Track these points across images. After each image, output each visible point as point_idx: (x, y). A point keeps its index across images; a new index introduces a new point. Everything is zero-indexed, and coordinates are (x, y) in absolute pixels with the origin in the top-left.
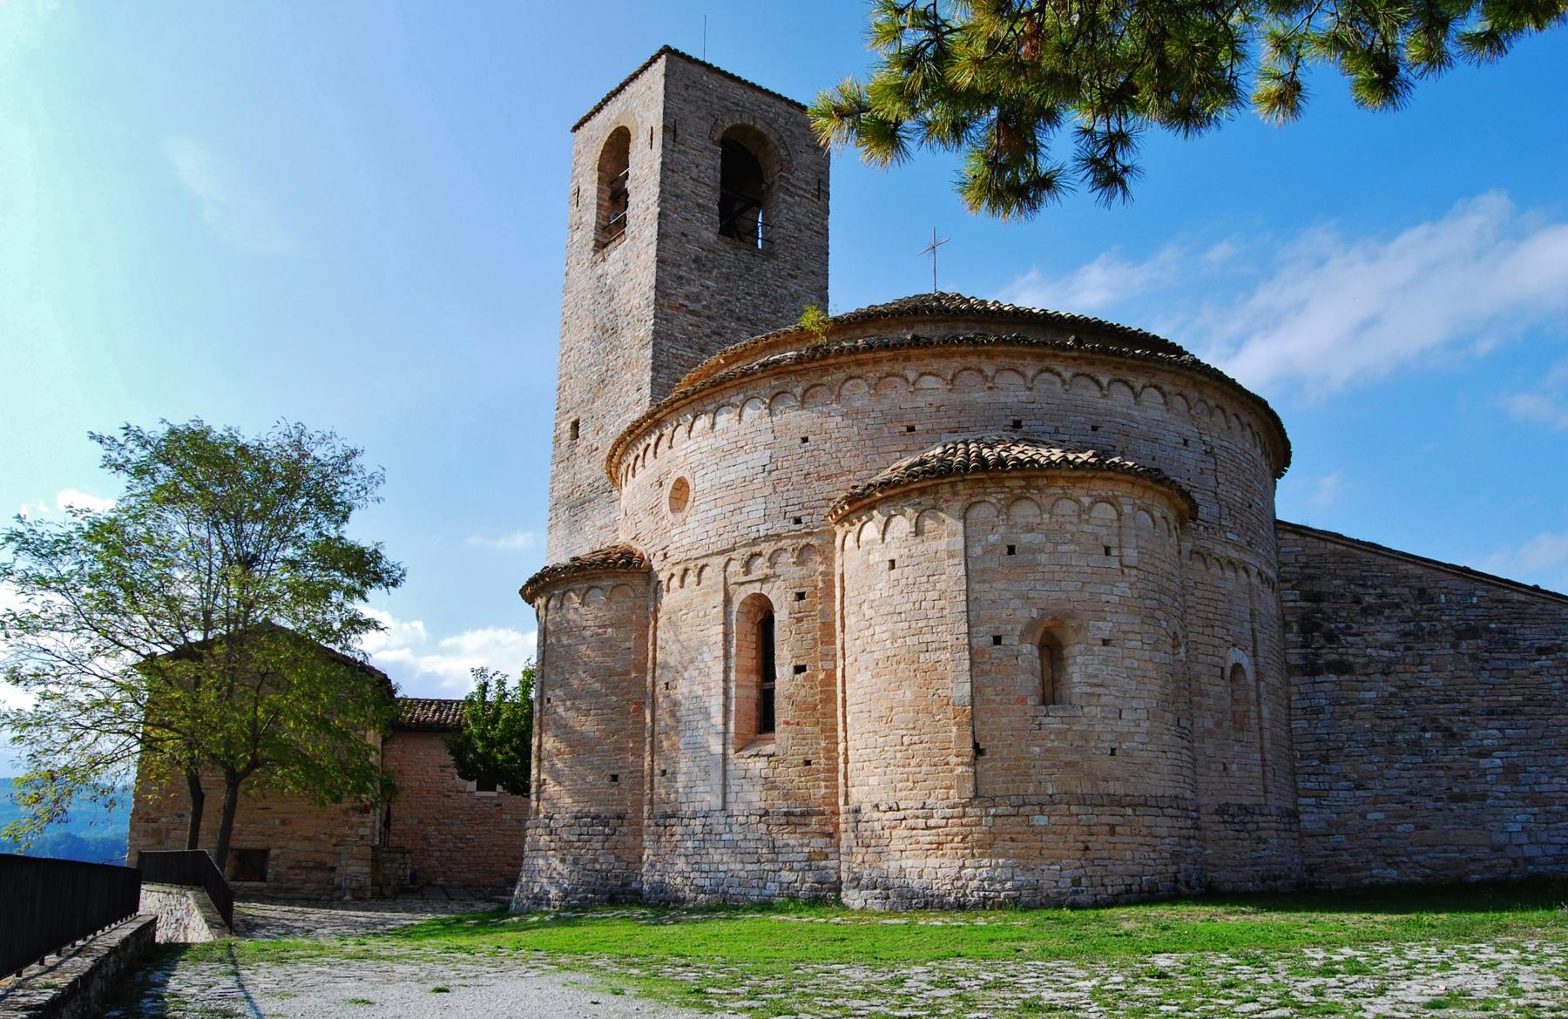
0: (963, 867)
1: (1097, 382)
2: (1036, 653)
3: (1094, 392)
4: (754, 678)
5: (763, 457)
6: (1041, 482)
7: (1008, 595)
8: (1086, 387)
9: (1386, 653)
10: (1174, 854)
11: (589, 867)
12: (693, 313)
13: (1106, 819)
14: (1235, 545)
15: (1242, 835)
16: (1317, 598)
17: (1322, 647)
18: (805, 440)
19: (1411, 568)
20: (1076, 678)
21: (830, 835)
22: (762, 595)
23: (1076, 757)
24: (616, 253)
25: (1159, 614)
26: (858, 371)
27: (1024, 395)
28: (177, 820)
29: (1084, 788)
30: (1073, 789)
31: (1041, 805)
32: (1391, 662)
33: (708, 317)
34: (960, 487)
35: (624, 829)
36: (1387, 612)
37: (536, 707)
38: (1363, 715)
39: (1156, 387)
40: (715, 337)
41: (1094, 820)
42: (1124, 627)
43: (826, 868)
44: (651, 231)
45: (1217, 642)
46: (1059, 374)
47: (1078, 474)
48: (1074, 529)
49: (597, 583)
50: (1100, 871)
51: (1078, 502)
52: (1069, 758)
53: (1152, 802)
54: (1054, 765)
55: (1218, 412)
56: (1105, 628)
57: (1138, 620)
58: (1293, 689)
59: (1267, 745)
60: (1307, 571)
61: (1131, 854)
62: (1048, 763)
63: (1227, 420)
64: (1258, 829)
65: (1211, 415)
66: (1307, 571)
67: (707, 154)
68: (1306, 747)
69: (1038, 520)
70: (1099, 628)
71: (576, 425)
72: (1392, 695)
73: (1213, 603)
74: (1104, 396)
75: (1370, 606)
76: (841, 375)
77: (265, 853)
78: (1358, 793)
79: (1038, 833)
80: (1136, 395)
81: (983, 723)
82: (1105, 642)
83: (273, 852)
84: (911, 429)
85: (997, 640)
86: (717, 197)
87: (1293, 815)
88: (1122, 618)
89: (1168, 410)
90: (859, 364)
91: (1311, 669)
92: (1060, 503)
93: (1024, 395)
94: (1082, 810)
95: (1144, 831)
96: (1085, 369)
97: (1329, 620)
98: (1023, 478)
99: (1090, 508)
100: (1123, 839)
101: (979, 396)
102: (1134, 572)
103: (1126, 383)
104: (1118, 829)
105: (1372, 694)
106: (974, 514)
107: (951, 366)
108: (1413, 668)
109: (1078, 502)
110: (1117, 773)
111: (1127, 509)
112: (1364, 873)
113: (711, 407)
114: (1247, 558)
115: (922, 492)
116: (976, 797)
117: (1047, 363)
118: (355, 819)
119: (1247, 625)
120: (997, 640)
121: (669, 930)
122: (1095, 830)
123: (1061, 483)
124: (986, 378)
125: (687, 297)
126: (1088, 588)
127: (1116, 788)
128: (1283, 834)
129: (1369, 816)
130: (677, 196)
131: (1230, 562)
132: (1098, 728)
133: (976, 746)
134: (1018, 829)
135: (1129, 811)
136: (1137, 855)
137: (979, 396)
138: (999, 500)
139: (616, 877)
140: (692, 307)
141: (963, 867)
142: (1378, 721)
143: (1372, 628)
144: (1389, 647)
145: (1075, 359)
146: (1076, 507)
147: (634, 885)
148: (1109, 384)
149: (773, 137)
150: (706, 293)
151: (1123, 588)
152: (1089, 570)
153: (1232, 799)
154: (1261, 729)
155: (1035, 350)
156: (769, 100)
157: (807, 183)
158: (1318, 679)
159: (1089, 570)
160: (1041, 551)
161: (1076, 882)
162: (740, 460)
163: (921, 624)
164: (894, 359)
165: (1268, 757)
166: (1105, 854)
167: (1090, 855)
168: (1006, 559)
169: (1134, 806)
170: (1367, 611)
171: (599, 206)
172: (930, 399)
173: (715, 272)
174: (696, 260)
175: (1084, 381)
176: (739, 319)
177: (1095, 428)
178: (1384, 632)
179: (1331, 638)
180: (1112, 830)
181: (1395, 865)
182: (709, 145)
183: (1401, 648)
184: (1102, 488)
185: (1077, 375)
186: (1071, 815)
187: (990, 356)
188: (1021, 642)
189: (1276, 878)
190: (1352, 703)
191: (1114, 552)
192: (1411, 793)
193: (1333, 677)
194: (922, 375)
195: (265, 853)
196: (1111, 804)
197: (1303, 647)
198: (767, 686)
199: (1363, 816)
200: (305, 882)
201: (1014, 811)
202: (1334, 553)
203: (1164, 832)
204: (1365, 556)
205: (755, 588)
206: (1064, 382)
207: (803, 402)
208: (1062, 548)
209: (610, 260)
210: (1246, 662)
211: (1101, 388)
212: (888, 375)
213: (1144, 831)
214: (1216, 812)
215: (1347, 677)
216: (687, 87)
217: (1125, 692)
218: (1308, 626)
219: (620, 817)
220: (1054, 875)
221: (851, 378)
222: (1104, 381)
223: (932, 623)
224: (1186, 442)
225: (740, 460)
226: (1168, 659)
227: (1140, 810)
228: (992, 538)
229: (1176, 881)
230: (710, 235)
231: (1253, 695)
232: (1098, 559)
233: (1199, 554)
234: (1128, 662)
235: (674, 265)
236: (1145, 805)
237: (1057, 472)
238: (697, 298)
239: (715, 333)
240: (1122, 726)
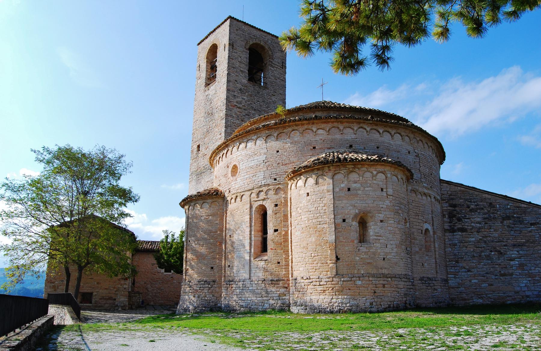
0: (332, 299)
1: (379, 132)
2: (358, 225)
4: (260, 234)
5: (263, 157)
6: (359, 166)
8: (374, 133)
9: (478, 225)
10: (405, 294)
11: (203, 299)
12: (239, 108)
13: (381, 282)
14: (426, 188)
15: (429, 288)
16: (454, 206)
17: (456, 223)
18: (278, 152)
19: (487, 196)
20: (371, 233)
21: (286, 288)
22: (263, 205)
24: (212, 87)
25: (400, 212)
26: (296, 128)
27: (353, 136)
29: (374, 271)
30: (370, 272)
31: (359, 277)
32: (480, 228)
33: (244, 109)
34: (331, 168)
35: (215, 286)
36: (478, 211)
37: (185, 244)
38: (470, 246)
39: (399, 133)
40: (247, 116)
41: (378, 282)
43: (285, 299)
44: (225, 80)
45: (420, 221)
46: (365, 129)
47: (372, 163)
48: (371, 182)
49: (206, 201)
51: (372, 173)
52: (369, 261)
53: (398, 276)
54: (364, 264)
55: (420, 142)
56: (381, 216)
58: (446, 237)
59: (437, 256)
60: (451, 197)
61: (390, 294)
62: (362, 263)
63: (423, 145)
64: (434, 286)
65: (418, 143)
66: (451, 197)
67: (244, 53)
68: (450, 257)
69: (358, 179)
71: (199, 146)
72: (480, 239)
73: (418, 208)
74: (381, 136)
75: (473, 209)
76: (290, 129)
77: (91, 294)
78: (468, 273)
79: (358, 287)
80: (392, 136)
81: (339, 249)
82: (381, 221)
83: (94, 294)
84: (314, 148)
85: (344, 221)
86: (247, 68)
87: (446, 281)
88: (387, 213)
89: (403, 141)
90: (297, 125)
91: (452, 230)
93: (353, 136)
94: (373, 279)
95: (395, 286)
96: (375, 127)
97: (458, 213)
98: (353, 165)
99: (376, 175)
101: (338, 136)
102: (391, 197)
103: (388, 132)
104: (386, 286)
105: (473, 239)
106: (336, 177)
107: (328, 126)
108: (488, 230)
109: (372, 173)
110: (386, 266)
111: (389, 175)
112: (471, 301)
113: (245, 140)
114: (430, 192)
115: (318, 169)
116: (337, 275)
117: (361, 125)
119: (430, 215)
120: (344, 221)
122: (378, 286)
123: (366, 166)
124: (340, 130)
125: (237, 102)
126: (375, 203)
127: (385, 271)
128: (443, 287)
129: (472, 281)
130: (233, 68)
131: (424, 194)
132: (379, 251)
133: (337, 257)
135: (390, 279)
136: (392, 295)
137: (338, 136)
138: (345, 172)
139: (213, 302)
140: (239, 106)
142: (475, 249)
143: (474, 216)
144: (479, 223)
145: (371, 124)
146: (371, 175)
147: (219, 305)
148: (383, 132)
149: (267, 47)
150: (244, 101)
151: (387, 202)
153: (425, 275)
154: (435, 251)
155: (357, 121)
156: (265, 34)
158: (455, 234)
159: (376, 196)
160: (359, 190)
161: (371, 304)
162: (255, 158)
163: (318, 215)
164: (309, 124)
165: (438, 261)
166: (381, 294)
167: (376, 294)
168: (347, 193)
169: (391, 278)
170: (472, 210)
171: (207, 71)
172: (321, 137)
173: (247, 94)
174: (240, 90)
175: (374, 131)
176: (255, 110)
178: (477, 218)
179: (459, 220)
180: (384, 286)
181: (481, 298)
182: (245, 50)
183: (483, 223)
184: (380, 168)
185: (372, 129)
186: (370, 281)
187: (342, 123)
188: (352, 221)
189: (440, 303)
190: (466, 242)
191: (384, 190)
192: (487, 273)
193: (460, 233)
194: (318, 129)
196: (383, 277)
197: (449, 223)
198: (265, 236)
199: (470, 281)
200: (105, 304)
201: (350, 279)
202: (460, 191)
203: (402, 286)
204: (471, 192)
205: (261, 203)
206: (367, 132)
207: (277, 139)
208: (367, 189)
209: (210, 89)
210: (430, 228)
211: (380, 134)
212: (306, 129)
213: (395, 286)
214: (420, 280)
215: (465, 233)
216: (237, 30)
217: (388, 238)
218: (451, 216)
219: (214, 281)
220: (363, 301)
221: (294, 130)
222: (381, 131)
223: (321, 214)
224: (409, 152)
225: (255, 158)
226: (403, 227)
227: (393, 279)
228: (342, 185)
229: (406, 303)
230: (245, 81)
231: (432, 240)
232: (379, 193)
233: (414, 191)
234: (389, 228)
235: (233, 91)
237: (365, 163)
238: (240, 103)
239: (247, 115)
240: (387, 250)
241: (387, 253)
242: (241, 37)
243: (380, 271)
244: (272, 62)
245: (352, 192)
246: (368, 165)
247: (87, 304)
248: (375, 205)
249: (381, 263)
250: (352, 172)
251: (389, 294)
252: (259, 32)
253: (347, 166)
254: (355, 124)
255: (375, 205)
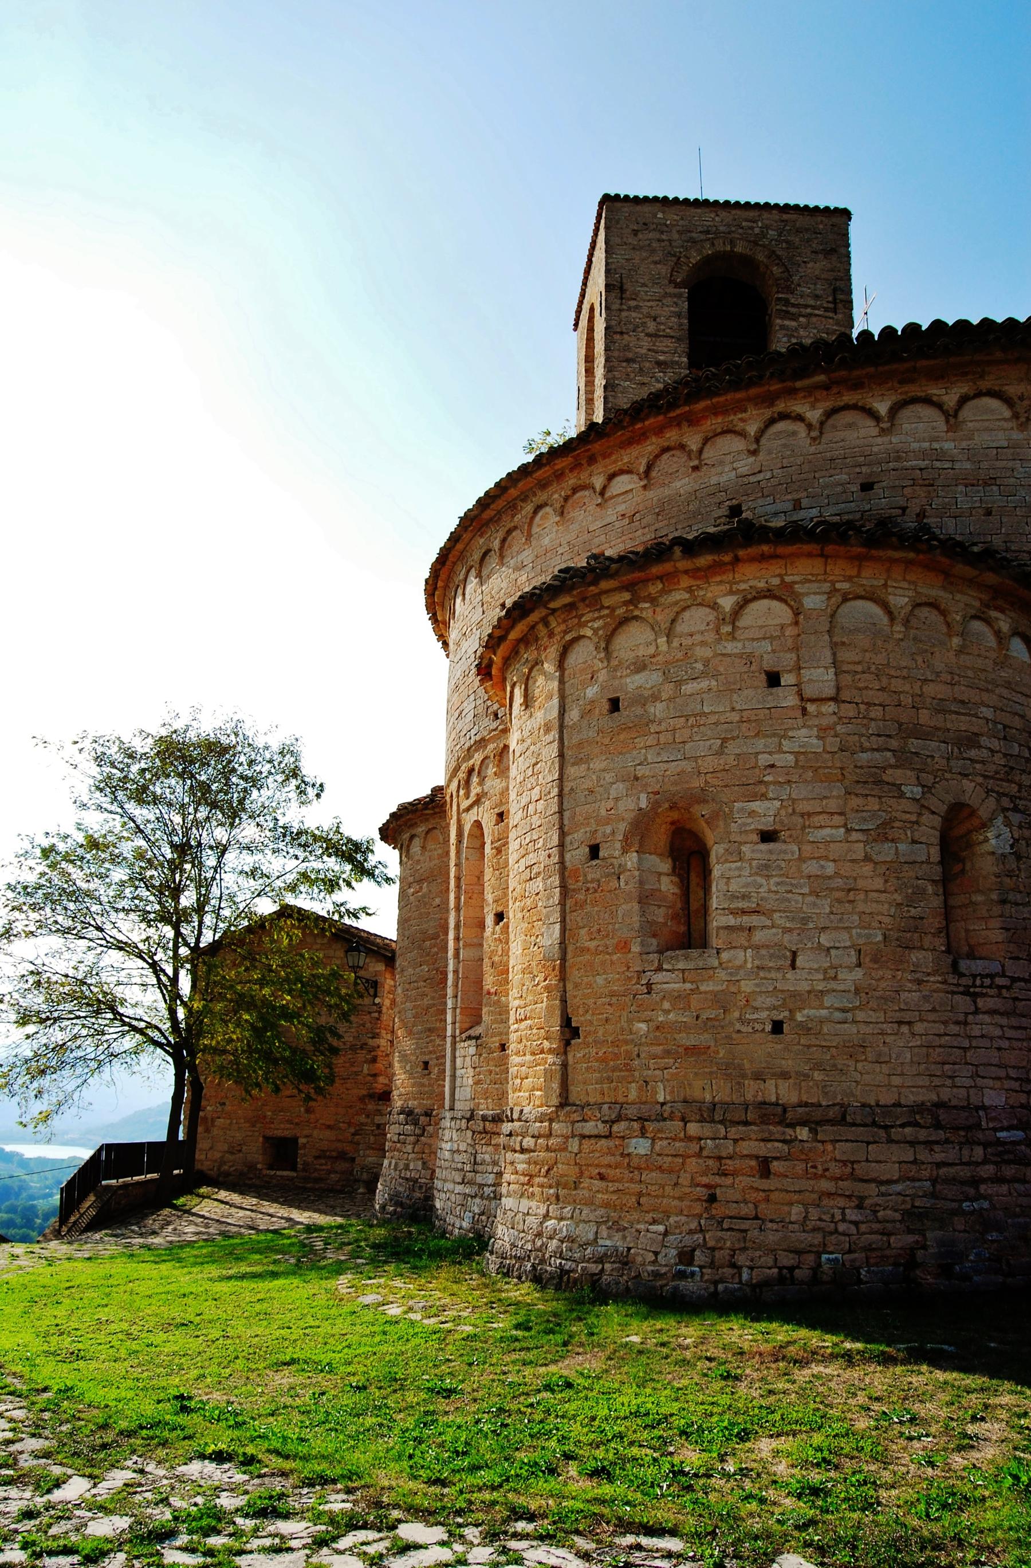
0: (546, 1216)
3: (867, 429)
6: (654, 588)
7: (609, 777)
8: (850, 426)
13: (747, 1147)
23: (704, 1039)
27: (746, 464)
28: (220, 1109)
29: (718, 1091)
30: (697, 1094)
39: (991, 394)
41: (729, 1148)
42: (803, 807)
48: (708, 653)
50: (729, 1240)
52: (691, 1040)
54: (667, 1053)
56: (765, 812)
57: (838, 790)
61: (799, 1209)
62: (658, 1050)
67: (668, 301)
69: (652, 650)
70: (752, 814)
74: (883, 432)
76: (529, 508)
77: (295, 1140)
79: (635, 1167)
81: (576, 986)
82: (768, 837)
83: (302, 1141)
85: (594, 851)
86: (684, 347)
88: (798, 791)
92: (686, 615)
93: (746, 464)
94: (707, 1130)
95: (836, 1170)
96: (848, 398)
100: (787, 1183)
103: (928, 401)
104: (775, 1165)
107: (639, 455)
109: (714, 606)
110: (788, 1064)
116: (562, 1106)
117: (781, 406)
118: (371, 1107)
120: (594, 851)
121: (276, 1282)
122: (730, 1165)
123: (685, 582)
126: (733, 748)
127: (785, 1092)
130: (628, 361)
132: (747, 986)
133: (566, 1022)
134: (608, 1159)
135: (803, 1133)
136: (814, 1214)
138: (595, 631)
141: (546, 1216)
145: (826, 387)
146: (712, 616)
149: (761, 257)
151: (805, 737)
152: (735, 717)
157: (817, 297)
159: (735, 717)
160: (656, 698)
161: (686, 1256)
164: (576, 466)
166: (747, 1210)
167: (718, 1210)
168: (608, 722)
169: (813, 1125)
175: (848, 417)
177: (867, 487)
182: (671, 290)
184: (754, 576)
187: (692, 420)
188: (625, 851)
191: (787, 679)
195: (295, 1140)
196: (764, 1120)
200: (329, 1172)
203: (891, 1171)
206: (810, 426)
208: (689, 688)
212: (575, 490)
213: (836, 1170)
217: (805, 921)
220: (651, 1244)
222: (882, 408)
227: (826, 1132)
228: (591, 692)
229: (912, 1263)
232: (753, 696)
234: (811, 868)
236: (842, 1120)
240: (796, 982)
241: (794, 995)
242: (653, 251)
243: (752, 1091)
244: (787, 303)
245: (626, 713)
246: (694, 573)
247: (285, 1173)
248: (731, 760)
249: (762, 1049)
250: (624, 621)
251: (796, 1212)
252: (723, 214)
253: (607, 601)
254: (752, 411)
255: (731, 760)
